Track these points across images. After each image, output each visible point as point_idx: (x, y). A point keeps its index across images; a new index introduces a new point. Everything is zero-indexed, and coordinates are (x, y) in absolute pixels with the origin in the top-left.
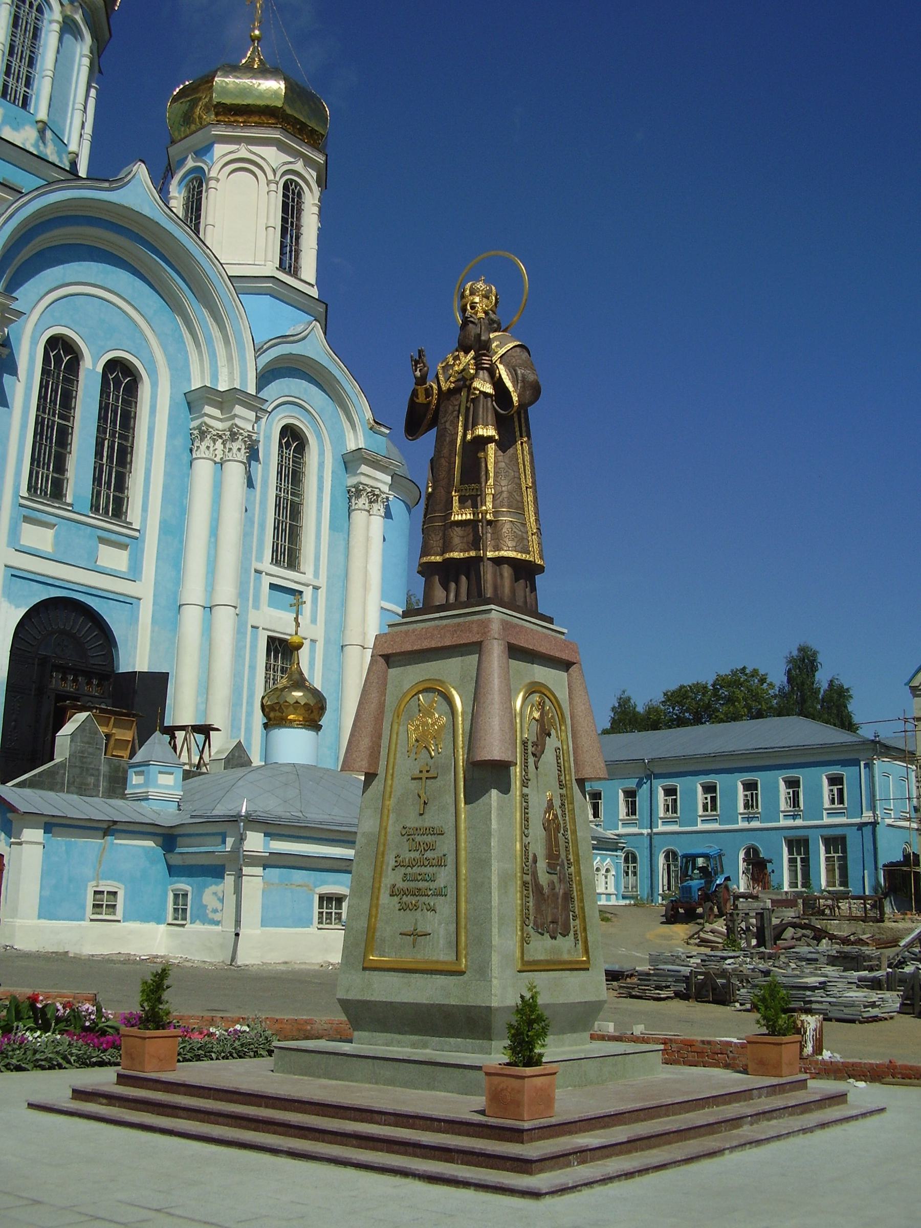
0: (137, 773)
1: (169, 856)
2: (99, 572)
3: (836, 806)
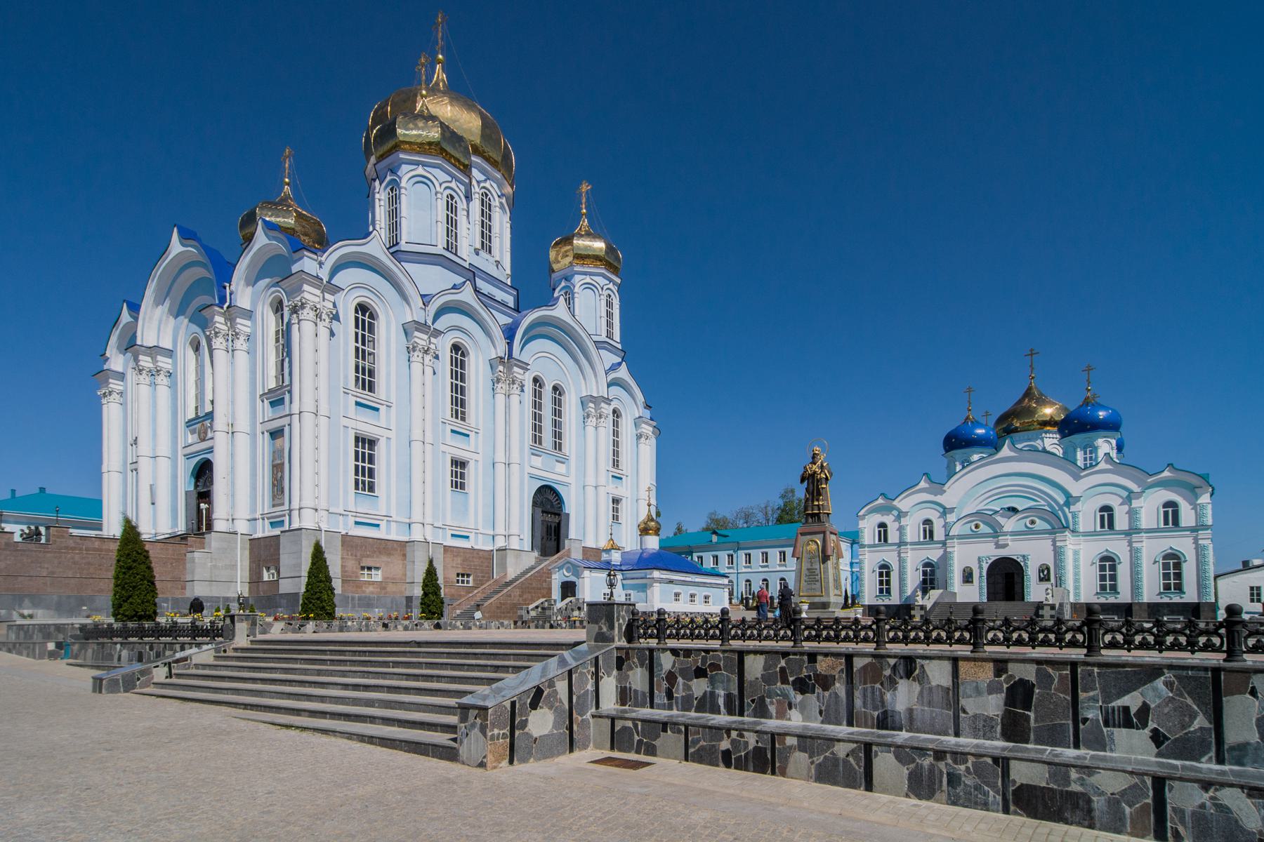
2: (556, 474)
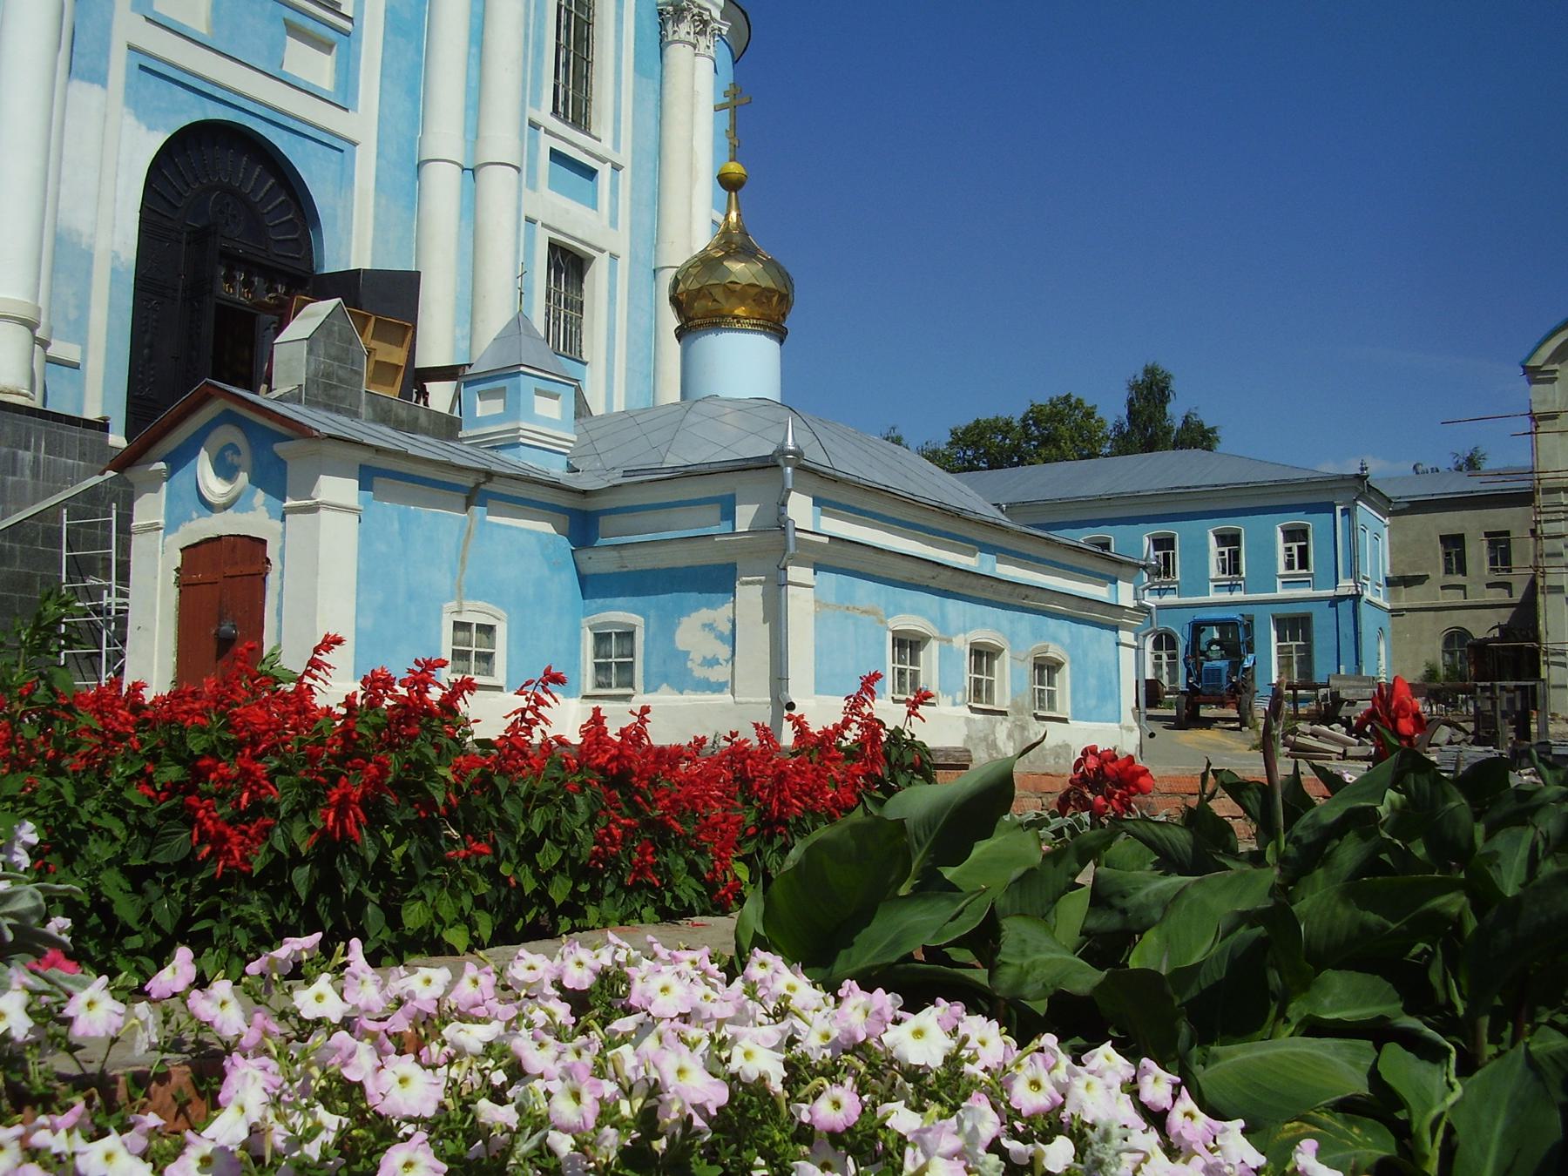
0: (483, 396)
1: (583, 555)
3: (1296, 571)
